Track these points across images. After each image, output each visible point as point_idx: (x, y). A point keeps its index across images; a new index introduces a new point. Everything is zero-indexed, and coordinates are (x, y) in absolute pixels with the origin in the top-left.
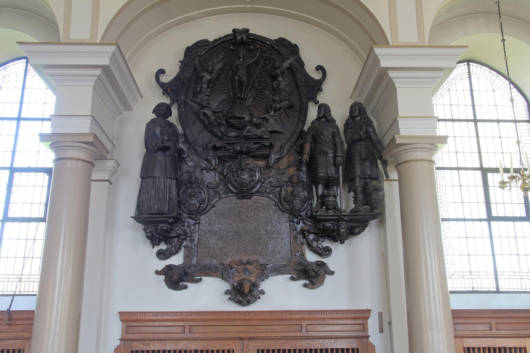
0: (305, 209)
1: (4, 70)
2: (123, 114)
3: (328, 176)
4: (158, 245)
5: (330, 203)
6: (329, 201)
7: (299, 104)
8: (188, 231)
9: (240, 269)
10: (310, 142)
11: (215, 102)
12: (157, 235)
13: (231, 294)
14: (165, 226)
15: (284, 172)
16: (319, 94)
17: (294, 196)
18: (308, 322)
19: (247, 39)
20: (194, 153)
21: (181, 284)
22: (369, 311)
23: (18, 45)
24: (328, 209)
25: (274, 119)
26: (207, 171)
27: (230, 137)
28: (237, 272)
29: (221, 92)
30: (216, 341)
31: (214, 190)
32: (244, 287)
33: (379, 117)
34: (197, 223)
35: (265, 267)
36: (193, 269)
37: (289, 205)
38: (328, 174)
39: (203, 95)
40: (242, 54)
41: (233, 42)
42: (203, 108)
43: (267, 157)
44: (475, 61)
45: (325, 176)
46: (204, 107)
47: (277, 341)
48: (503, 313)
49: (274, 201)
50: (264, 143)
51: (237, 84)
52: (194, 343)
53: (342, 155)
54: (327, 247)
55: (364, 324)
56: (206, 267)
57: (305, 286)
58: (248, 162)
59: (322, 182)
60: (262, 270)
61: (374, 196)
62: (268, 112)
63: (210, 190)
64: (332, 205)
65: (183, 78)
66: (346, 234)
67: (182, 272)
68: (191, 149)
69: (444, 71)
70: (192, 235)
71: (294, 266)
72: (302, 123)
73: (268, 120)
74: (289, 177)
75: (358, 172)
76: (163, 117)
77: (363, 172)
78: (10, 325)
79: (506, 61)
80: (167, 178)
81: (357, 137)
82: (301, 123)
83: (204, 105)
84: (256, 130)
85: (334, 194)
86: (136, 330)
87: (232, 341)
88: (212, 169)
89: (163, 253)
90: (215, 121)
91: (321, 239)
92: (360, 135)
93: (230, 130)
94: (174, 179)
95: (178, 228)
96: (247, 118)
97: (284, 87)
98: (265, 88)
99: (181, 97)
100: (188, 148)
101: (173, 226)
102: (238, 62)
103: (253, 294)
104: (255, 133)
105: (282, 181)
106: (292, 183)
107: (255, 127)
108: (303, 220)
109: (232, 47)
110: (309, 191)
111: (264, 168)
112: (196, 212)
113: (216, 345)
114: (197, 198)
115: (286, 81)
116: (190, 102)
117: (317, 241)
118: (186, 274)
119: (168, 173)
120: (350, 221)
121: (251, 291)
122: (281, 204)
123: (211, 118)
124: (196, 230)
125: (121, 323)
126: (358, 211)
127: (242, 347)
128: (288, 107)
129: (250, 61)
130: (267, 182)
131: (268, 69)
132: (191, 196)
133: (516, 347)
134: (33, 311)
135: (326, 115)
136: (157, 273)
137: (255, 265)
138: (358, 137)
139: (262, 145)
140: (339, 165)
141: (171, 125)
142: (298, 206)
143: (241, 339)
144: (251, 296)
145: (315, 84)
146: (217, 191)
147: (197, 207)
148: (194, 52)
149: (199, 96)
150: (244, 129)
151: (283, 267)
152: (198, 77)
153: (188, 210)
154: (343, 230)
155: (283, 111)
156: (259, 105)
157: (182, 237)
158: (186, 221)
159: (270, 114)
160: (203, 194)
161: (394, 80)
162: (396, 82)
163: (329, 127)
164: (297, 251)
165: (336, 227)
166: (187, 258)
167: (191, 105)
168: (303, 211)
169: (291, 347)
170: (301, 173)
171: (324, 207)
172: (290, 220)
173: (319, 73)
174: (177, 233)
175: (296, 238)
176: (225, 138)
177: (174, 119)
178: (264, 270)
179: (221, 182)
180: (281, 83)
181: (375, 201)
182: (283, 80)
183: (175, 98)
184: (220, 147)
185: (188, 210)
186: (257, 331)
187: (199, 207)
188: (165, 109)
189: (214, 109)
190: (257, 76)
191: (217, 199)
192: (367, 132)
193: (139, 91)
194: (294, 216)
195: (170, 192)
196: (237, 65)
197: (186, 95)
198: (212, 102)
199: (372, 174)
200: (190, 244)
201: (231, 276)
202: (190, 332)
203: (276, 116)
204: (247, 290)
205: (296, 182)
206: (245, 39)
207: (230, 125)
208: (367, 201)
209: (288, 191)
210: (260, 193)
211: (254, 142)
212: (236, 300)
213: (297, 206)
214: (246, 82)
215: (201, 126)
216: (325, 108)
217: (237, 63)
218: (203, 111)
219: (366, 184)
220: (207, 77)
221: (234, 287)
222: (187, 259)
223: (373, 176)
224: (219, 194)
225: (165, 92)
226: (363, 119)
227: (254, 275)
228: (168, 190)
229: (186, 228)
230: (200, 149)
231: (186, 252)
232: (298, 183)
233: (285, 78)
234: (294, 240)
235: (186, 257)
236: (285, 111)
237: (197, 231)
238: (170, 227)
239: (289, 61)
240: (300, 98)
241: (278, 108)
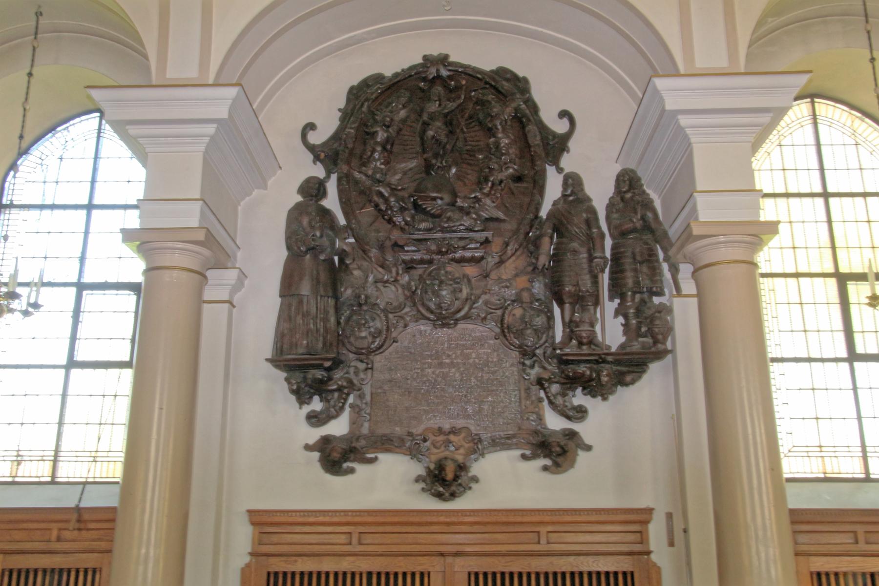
13: (424, 481)
18: (550, 528)
22: (650, 511)
47: (500, 558)
54: (580, 406)
57: (545, 468)
80: (321, 296)
86: (275, 538)
120: (618, 362)
121: (456, 477)
136: (308, 448)
137: (463, 435)
151: (508, 438)
166: (354, 424)
169: (523, 568)
174: (338, 384)
195: (326, 320)
200: (359, 403)
204: (450, 476)
225: (317, 158)
227: (462, 451)
235: (353, 423)
238: (326, 375)
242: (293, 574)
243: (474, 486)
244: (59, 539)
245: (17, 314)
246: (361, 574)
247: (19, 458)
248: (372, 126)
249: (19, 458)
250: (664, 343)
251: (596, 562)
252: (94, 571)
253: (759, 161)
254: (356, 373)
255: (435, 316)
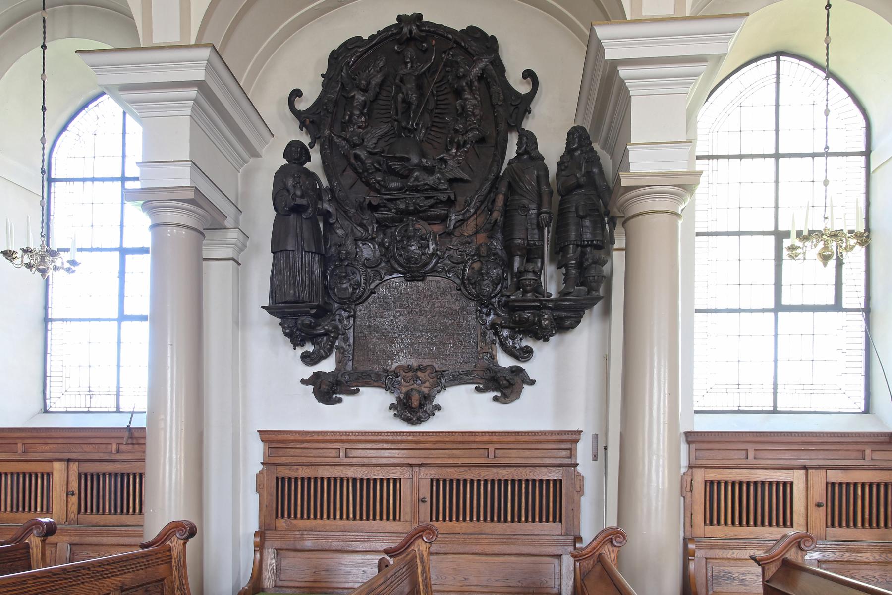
0: (497, 294)
1: (97, 107)
2: (249, 163)
3: (528, 244)
4: (303, 346)
5: (527, 283)
6: (526, 280)
7: (494, 134)
8: (340, 327)
9: (408, 377)
10: (503, 193)
11: (373, 137)
12: (297, 332)
13: (396, 408)
14: (307, 320)
15: (470, 241)
16: (528, 118)
17: (482, 274)
18: (497, 446)
19: (418, 31)
20: (345, 215)
21: (334, 396)
22: (579, 432)
23: (77, 55)
24: (525, 292)
25: (456, 160)
26: (364, 243)
27: (390, 190)
28: (405, 381)
29: (382, 122)
30: (379, 467)
31: (372, 269)
32: (411, 400)
33: (613, 150)
34: (352, 316)
35: (442, 374)
36: (347, 377)
37: (475, 289)
38: (528, 241)
39: (355, 127)
40: (410, 56)
41: (398, 38)
42: (354, 147)
43: (444, 219)
44: (789, 54)
45: (524, 244)
46: (354, 146)
47: (456, 469)
48: (767, 436)
49: (455, 283)
50: (438, 197)
51: (400, 106)
52: (352, 470)
53: (548, 210)
54: (526, 347)
55: (571, 449)
56: (365, 374)
57: (495, 399)
58: (417, 226)
59: (519, 253)
60: (437, 378)
61: (593, 272)
62: (448, 150)
63: (368, 269)
64: (530, 286)
65: (326, 101)
66: (551, 328)
67: (333, 380)
68: (340, 210)
69: (709, 62)
70: (346, 332)
71: (481, 373)
72: (497, 165)
73: (447, 162)
74: (476, 248)
75: (573, 235)
76: (296, 161)
77: (580, 236)
78: (133, 444)
79: (828, 44)
80: (305, 252)
81: (573, 181)
82: (495, 164)
83: (355, 142)
84: (428, 177)
85: (533, 269)
86: (281, 452)
87: (399, 468)
88: (370, 239)
89: (309, 356)
90: (372, 167)
91: (519, 337)
92: (578, 179)
93: (391, 179)
94: (315, 253)
95: (326, 323)
96: (415, 160)
97: (472, 108)
98: (444, 112)
99: (323, 132)
100: (337, 209)
101: (320, 319)
102: (405, 70)
103: (425, 409)
104: (425, 182)
105: (467, 255)
106: (479, 256)
107: (427, 173)
108: (495, 309)
109: (396, 47)
110: (504, 268)
111: (442, 235)
112: (349, 301)
113: (379, 472)
114: (350, 280)
115: (476, 98)
116: (335, 138)
117: (513, 339)
118: (339, 383)
119: (306, 245)
120: (556, 308)
121: (421, 405)
122: (465, 287)
123: (367, 162)
124: (351, 325)
125: (262, 444)
126: (569, 294)
127: (411, 475)
128: (478, 140)
129: (422, 68)
130: (446, 256)
131: (449, 80)
132: (341, 278)
133: (779, 480)
134: (144, 428)
135: (529, 149)
136: (303, 382)
137: (428, 371)
138: (573, 182)
139: (438, 201)
140: (543, 227)
141: (312, 176)
142: (488, 290)
143: (410, 465)
144: (422, 412)
145: (519, 101)
146: (377, 271)
147: (350, 294)
148: (342, 59)
149: (348, 129)
150: (410, 177)
151: (466, 374)
152: (347, 98)
153: (339, 298)
154: (545, 321)
155: (470, 147)
156: (435, 140)
157: (332, 335)
158: (337, 313)
159: (451, 152)
160: (358, 275)
161: (628, 83)
162: (632, 86)
163: (532, 168)
164: (485, 352)
165: (537, 319)
166: (340, 363)
167: (338, 143)
168: (495, 296)
169: (474, 476)
170: (493, 242)
171: (521, 290)
172: (477, 310)
173: (528, 83)
174: (325, 329)
175: (484, 335)
176: (383, 191)
177: (315, 163)
178: (440, 378)
179: (382, 257)
180: (467, 102)
181: (593, 278)
182: (472, 97)
183: (317, 135)
184: (378, 205)
185: (339, 298)
186: (430, 456)
187: (353, 293)
188: (299, 149)
189: (371, 148)
190: (432, 92)
191: (377, 282)
192: (589, 174)
193: (266, 125)
194: (483, 304)
195: (311, 273)
196: (402, 75)
197: (331, 129)
198: (368, 136)
199: (593, 239)
200: (343, 345)
201: (397, 386)
202: (346, 457)
203: (460, 155)
204: (415, 403)
205: (485, 255)
206: (415, 31)
207: (391, 172)
208: (583, 280)
209: (474, 268)
210: (435, 273)
211: (425, 196)
212: (403, 416)
213: (486, 290)
214: (416, 102)
215: (353, 175)
216: (527, 139)
217: (402, 72)
218: (354, 152)
219: (583, 254)
220: (360, 97)
221: (399, 399)
222: (340, 364)
223: (595, 242)
224: (380, 275)
225: (302, 126)
226: (584, 154)
227: (427, 384)
228: (307, 269)
229: (337, 322)
230: (353, 210)
231: (338, 354)
232: (488, 256)
233: (474, 94)
234: (482, 338)
235: (339, 362)
236: (473, 147)
237: (351, 327)
238: (313, 321)
239: (481, 65)
240: (497, 125)
241: (462, 143)
242: (296, 478)
243: (437, 413)
244: (118, 452)
245: (62, 270)
246: (348, 480)
247: (91, 393)
248: (351, 91)
249: (91, 393)
250: (597, 290)
251: (532, 472)
252: (48, 474)
253: (707, 115)
254: (341, 321)
255: (405, 270)
